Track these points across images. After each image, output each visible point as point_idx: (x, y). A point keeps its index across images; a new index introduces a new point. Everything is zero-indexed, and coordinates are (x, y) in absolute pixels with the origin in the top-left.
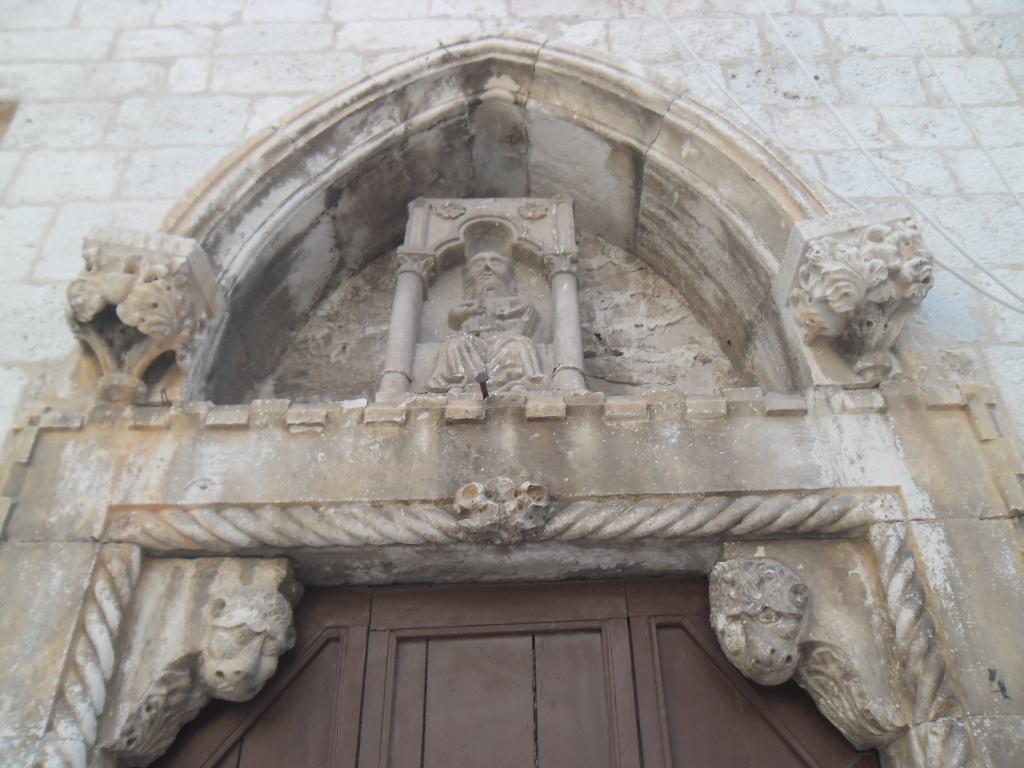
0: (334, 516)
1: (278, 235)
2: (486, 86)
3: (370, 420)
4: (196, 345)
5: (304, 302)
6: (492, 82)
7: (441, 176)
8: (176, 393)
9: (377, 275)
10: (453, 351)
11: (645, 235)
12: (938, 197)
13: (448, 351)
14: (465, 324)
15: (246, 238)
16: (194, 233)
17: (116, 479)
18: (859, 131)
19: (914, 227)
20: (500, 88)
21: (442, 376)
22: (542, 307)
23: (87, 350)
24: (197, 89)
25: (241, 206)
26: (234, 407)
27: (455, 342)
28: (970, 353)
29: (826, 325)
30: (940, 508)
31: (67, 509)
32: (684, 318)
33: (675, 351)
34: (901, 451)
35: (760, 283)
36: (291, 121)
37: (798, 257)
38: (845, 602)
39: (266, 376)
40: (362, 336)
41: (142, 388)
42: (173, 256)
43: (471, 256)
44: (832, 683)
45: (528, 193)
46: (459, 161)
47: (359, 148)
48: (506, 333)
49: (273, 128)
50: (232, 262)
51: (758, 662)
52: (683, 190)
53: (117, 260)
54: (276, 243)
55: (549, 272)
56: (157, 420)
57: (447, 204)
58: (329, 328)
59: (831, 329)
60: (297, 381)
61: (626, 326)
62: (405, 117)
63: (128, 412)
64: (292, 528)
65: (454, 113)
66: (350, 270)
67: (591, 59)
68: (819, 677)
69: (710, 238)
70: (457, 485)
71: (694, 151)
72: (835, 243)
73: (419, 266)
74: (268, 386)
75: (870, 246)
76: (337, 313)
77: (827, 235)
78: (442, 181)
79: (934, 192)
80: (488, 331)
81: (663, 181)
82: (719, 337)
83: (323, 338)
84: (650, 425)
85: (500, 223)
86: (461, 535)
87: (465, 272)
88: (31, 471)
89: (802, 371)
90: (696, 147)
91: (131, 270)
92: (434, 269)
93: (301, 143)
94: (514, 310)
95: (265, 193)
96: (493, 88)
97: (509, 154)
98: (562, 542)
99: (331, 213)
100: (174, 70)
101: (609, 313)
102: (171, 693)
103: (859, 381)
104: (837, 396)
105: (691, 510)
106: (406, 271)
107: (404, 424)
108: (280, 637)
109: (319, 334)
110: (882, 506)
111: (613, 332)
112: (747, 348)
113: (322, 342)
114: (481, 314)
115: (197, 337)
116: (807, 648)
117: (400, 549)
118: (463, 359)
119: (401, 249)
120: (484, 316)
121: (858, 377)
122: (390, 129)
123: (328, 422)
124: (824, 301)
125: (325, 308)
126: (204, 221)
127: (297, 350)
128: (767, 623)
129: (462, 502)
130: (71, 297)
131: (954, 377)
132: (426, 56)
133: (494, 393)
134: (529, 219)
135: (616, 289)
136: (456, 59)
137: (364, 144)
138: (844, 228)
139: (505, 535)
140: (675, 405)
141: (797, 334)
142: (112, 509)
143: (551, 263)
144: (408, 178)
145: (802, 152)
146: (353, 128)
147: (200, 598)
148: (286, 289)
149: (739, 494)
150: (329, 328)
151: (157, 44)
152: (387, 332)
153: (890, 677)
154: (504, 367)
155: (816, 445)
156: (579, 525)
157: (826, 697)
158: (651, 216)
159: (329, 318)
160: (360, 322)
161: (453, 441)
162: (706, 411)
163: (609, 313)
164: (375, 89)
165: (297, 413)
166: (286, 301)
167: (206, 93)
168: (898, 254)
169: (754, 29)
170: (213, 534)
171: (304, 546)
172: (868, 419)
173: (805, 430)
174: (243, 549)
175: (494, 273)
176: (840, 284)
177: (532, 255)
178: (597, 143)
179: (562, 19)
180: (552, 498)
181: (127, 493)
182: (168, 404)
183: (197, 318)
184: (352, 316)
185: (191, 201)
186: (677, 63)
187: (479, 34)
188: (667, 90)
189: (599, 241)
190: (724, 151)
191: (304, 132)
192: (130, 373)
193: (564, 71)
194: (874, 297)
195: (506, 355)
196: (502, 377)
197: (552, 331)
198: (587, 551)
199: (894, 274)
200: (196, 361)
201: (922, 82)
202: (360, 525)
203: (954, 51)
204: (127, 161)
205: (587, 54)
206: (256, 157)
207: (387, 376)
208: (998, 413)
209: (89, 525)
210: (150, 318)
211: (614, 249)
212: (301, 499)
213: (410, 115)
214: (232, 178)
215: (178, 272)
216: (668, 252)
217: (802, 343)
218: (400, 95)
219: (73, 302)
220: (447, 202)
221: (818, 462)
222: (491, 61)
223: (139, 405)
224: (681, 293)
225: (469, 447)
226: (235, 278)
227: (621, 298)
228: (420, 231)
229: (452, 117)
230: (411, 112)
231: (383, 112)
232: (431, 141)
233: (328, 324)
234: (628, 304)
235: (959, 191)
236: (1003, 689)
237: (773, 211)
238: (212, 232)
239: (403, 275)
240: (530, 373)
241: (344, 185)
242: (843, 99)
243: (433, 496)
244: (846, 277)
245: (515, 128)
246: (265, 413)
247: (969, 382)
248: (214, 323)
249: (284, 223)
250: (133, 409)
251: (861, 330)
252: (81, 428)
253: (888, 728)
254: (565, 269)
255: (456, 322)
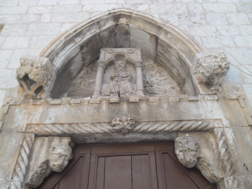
0: (82, 126)
1: (68, 57)
2: (120, 20)
3: (91, 103)
4: (48, 84)
5: (75, 74)
6: (121, 19)
7: (108, 42)
8: (43, 96)
9: (93, 67)
10: (111, 86)
11: (159, 57)
12: (231, 48)
13: (110, 86)
14: (114, 79)
15: (60, 58)
16: (48, 56)
17: (28, 117)
18: (211, 31)
19: (225, 55)
20: (123, 21)
21: (109, 92)
22: (133, 75)
23: (21, 85)
24: (48, 21)
25: (59, 50)
26: (58, 99)
27: (112, 83)
28: (239, 86)
29: (203, 79)
30: (231, 124)
31: (16, 125)
32: (168, 77)
33: (166, 86)
34: (222, 110)
35: (187, 69)
36: (72, 28)
37: (196, 62)
38: (208, 147)
39: (65, 92)
40: (89, 82)
41: (35, 95)
42: (42, 62)
43: (116, 62)
44: (205, 167)
45: (130, 47)
46: (113, 39)
47: (88, 36)
48: (125, 81)
49: (67, 31)
50: (57, 64)
51: (187, 162)
52: (168, 46)
53: (29, 63)
54: (68, 59)
55: (135, 66)
56: (38, 102)
57: (110, 50)
58: (81, 80)
59: (205, 80)
60: (73, 93)
61: (154, 79)
62: (100, 28)
63: (31, 101)
64: (72, 129)
65: (112, 27)
66: (86, 66)
67: (145, 14)
68: (202, 166)
69: (175, 58)
70: (112, 119)
71: (171, 36)
72: (205, 59)
73: (103, 65)
74: (66, 94)
75: (214, 59)
76: (83, 76)
77: (204, 57)
78: (109, 44)
79: (230, 46)
80: (120, 81)
81: (163, 44)
82: (177, 82)
83: (80, 82)
84: (160, 104)
85: (123, 54)
86: (113, 131)
87: (114, 66)
88: (7, 115)
89: (197, 90)
90: (171, 35)
91: (32, 66)
92: (107, 66)
93: (74, 34)
94: (126, 75)
95: (65, 47)
96: (121, 21)
97: (125, 37)
98: (138, 133)
99: (81, 52)
100: (43, 16)
101: (150, 76)
102: (42, 170)
103: (211, 93)
104: (206, 97)
105: (170, 124)
106: (100, 66)
107: (100, 103)
108: (69, 156)
109: (78, 82)
110: (217, 124)
111: (151, 81)
112: (184, 85)
113: (79, 84)
114: (118, 77)
115: (48, 82)
116: (199, 159)
117: (98, 134)
118: (114, 88)
119: (98, 60)
120: (119, 77)
121: (211, 92)
122: (96, 31)
123: (80, 103)
124: (203, 73)
125: (80, 75)
126: (50, 54)
127: (73, 85)
128: (189, 152)
129: (114, 123)
130: (17, 72)
131: (235, 92)
132: (104, 13)
133: (121, 96)
134: (130, 53)
135: (152, 71)
136: (112, 14)
137: (89, 35)
138: (208, 55)
139: (124, 131)
140: (166, 99)
141: (196, 81)
142: (27, 125)
143: (135, 64)
144: (100, 43)
145: (197, 36)
146: (87, 31)
147: (49, 146)
148: (70, 71)
149: (182, 121)
150: (81, 80)
151: (38, 10)
152: (95, 81)
153: (219, 166)
154: (124, 90)
155: (201, 109)
156: (142, 128)
157: (203, 170)
158: (160, 52)
159: (81, 78)
160: (88, 78)
161: (111, 108)
162: (174, 100)
163: (150, 76)
164: (92, 21)
165: (73, 101)
166: (70, 73)
167: (50, 22)
168: (221, 62)
169: (186, 7)
170: (52, 131)
171: (75, 134)
172: (214, 102)
173: (198, 105)
174: (60, 134)
175: (121, 66)
176: (207, 69)
177: (131, 62)
178: (147, 34)
179: (138, 4)
180: (136, 122)
181: (31, 121)
182: (41, 99)
183: (48, 78)
184: (86, 77)
185: (47, 49)
186: (167, 15)
187: (118, 7)
188: (164, 21)
189: (147, 59)
190: (178, 36)
191: (75, 32)
192: (32, 91)
193: (139, 17)
194: (215, 72)
195: (124, 87)
196: (123, 92)
197: (136, 81)
198: (144, 135)
199: (220, 66)
200: (48, 88)
201: (227, 19)
202: (88, 128)
203: (235, 12)
204: (31, 39)
205: (144, 12)
206: (63, 38)
207: (95, 92)
208: (246, 101)
209: (22, 128)
210: (37, 78)
211: (151, 60)
212: (74, 122)
213: (101, 28)
214: (57, 43)
215: (44, 66)
216: (164, 61)
217: (197, 84)
218: (98, 23)
219: (18, 73)
220: (110, 49)
221: (201, 113)
222: (121, 14)
223: (34, 99)
224: (168, 71)
225: (115, 109)
226: (58, 68)
227: (153, 73)
228: (101, 57)
229: (111, 28)
230: (101, 27)
231: (94, 27)
232: (106, 34)
233: (81, 79)
234: (155, 74)
235: (236, 46)
236: (247, 169)
237: (190, 51)
238: (52, 57)
239: (99, 67)
240: (130, 91)
241: (84, 45)
242: (208, 23)
243: (107, 121)
244: (208, 67)
245: (127, 31)
246: (65, 101)
247: (239, 93)
248: (52, 79)
249: (70, 54)
250: (32, 100)
251: (212, 80)
252: (20, 105)
253: (219, 178)
254: (139, 65)
255: (112, 79)
